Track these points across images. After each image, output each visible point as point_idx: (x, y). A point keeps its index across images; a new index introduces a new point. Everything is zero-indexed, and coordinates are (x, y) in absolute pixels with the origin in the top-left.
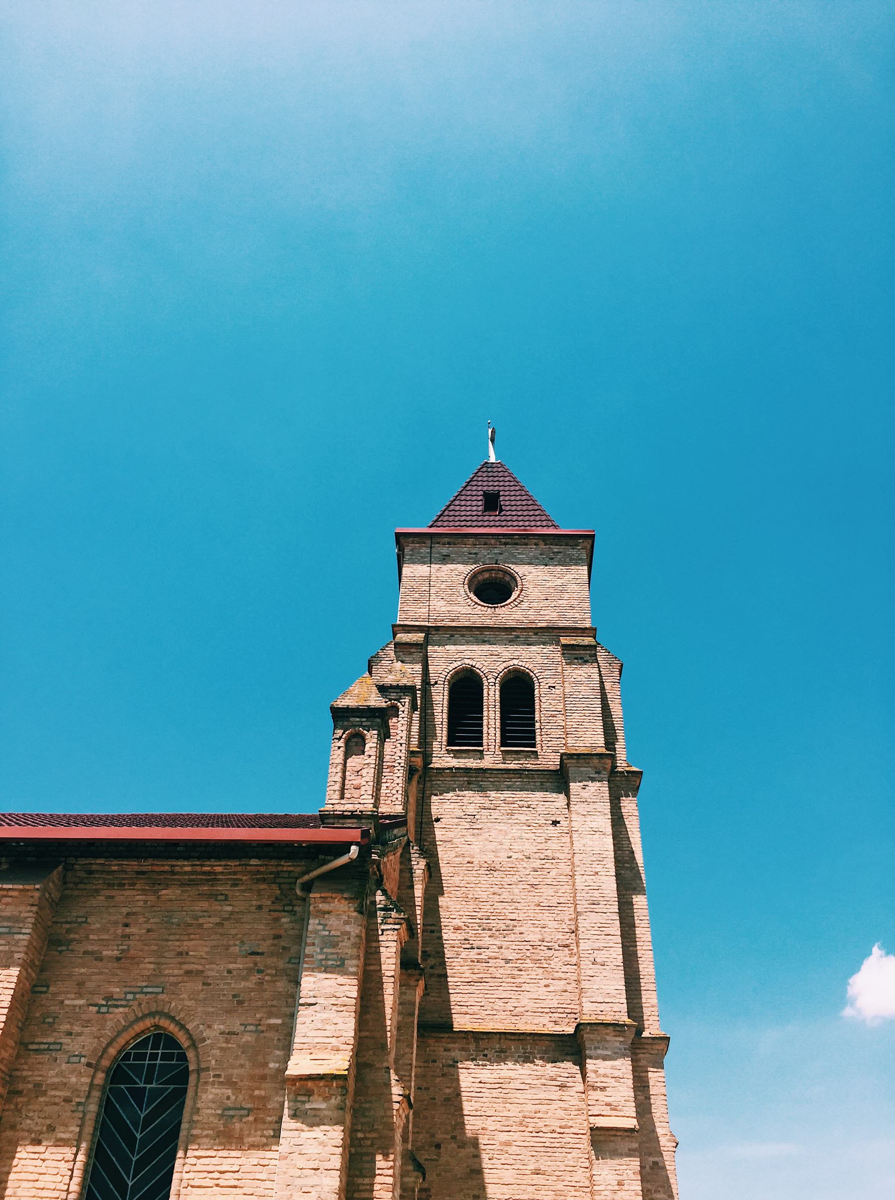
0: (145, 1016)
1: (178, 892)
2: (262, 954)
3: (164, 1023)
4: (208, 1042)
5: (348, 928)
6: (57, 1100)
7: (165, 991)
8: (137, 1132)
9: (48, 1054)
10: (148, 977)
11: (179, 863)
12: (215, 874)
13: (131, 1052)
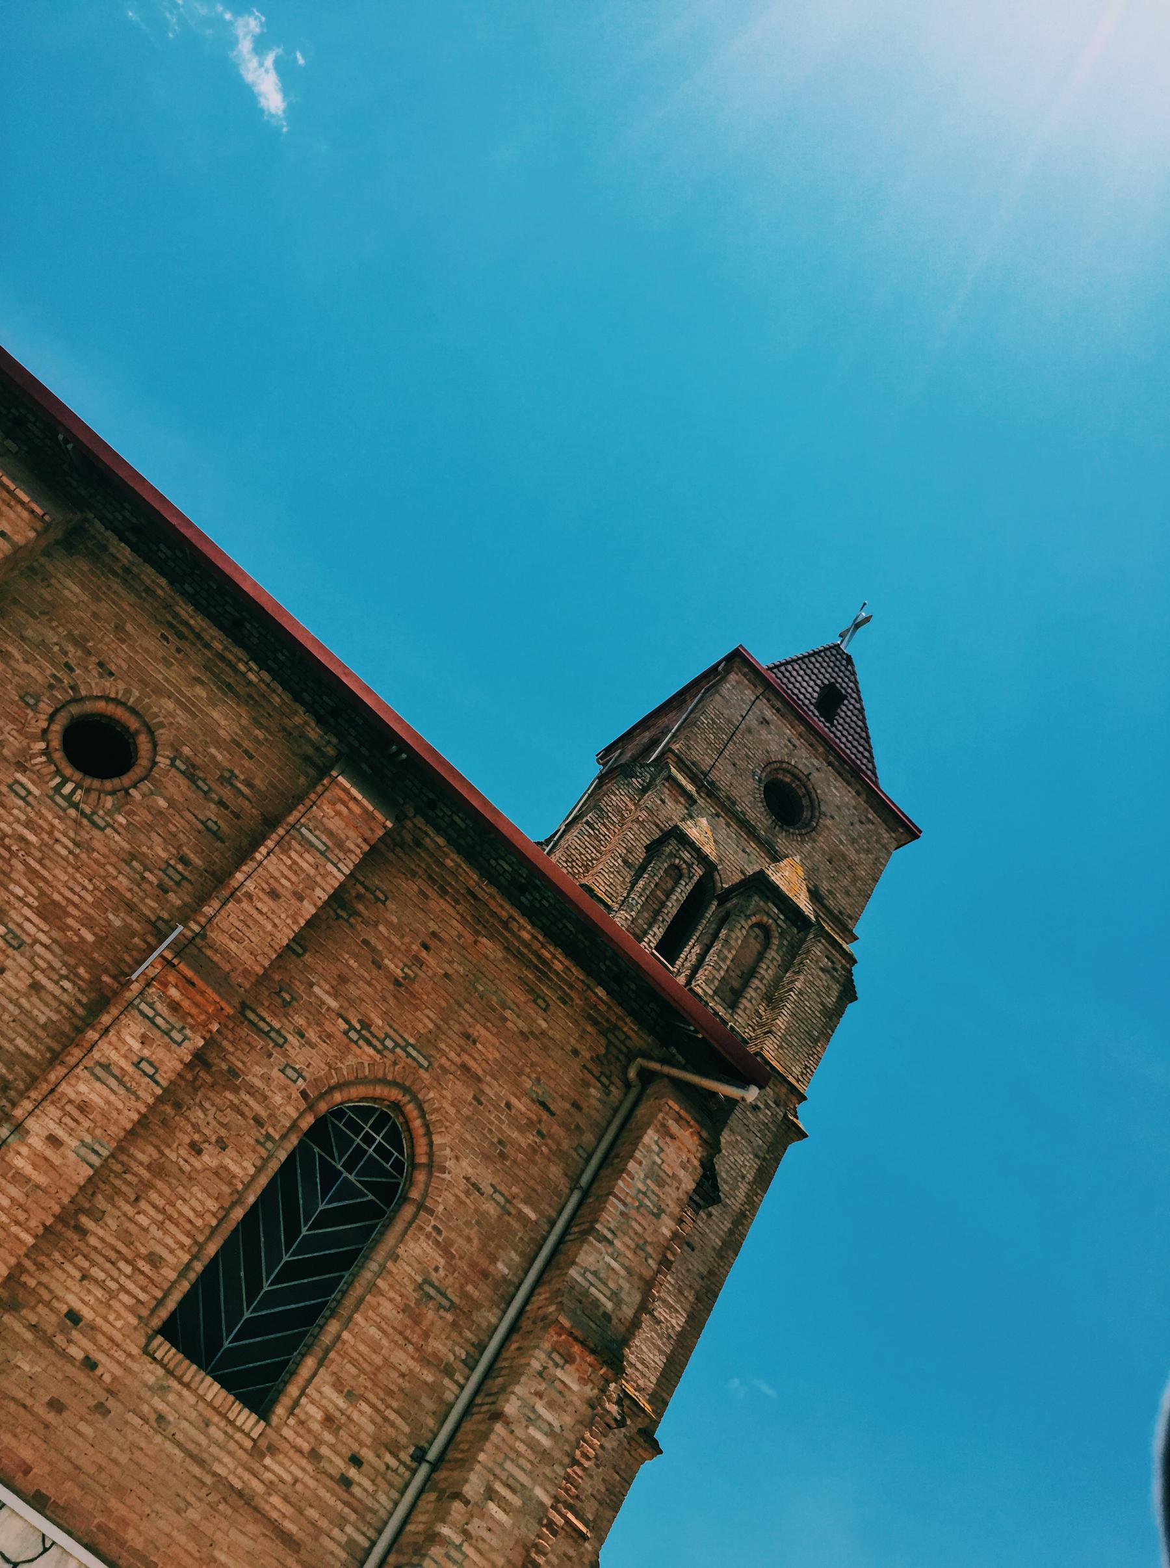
0: (394, 1084)
1: (500, 955)
2: (552, 1114)
3: (411, 1109)
4: (446, 1176)
5: (682, 1173)
6: (246, 1110)
7: (430, 1069)
8: (305, 1226)
9: (264, 1040)
10: (421, 1035)
11: (521, 921)
12: (550, 968)
13: (346, 1113)
